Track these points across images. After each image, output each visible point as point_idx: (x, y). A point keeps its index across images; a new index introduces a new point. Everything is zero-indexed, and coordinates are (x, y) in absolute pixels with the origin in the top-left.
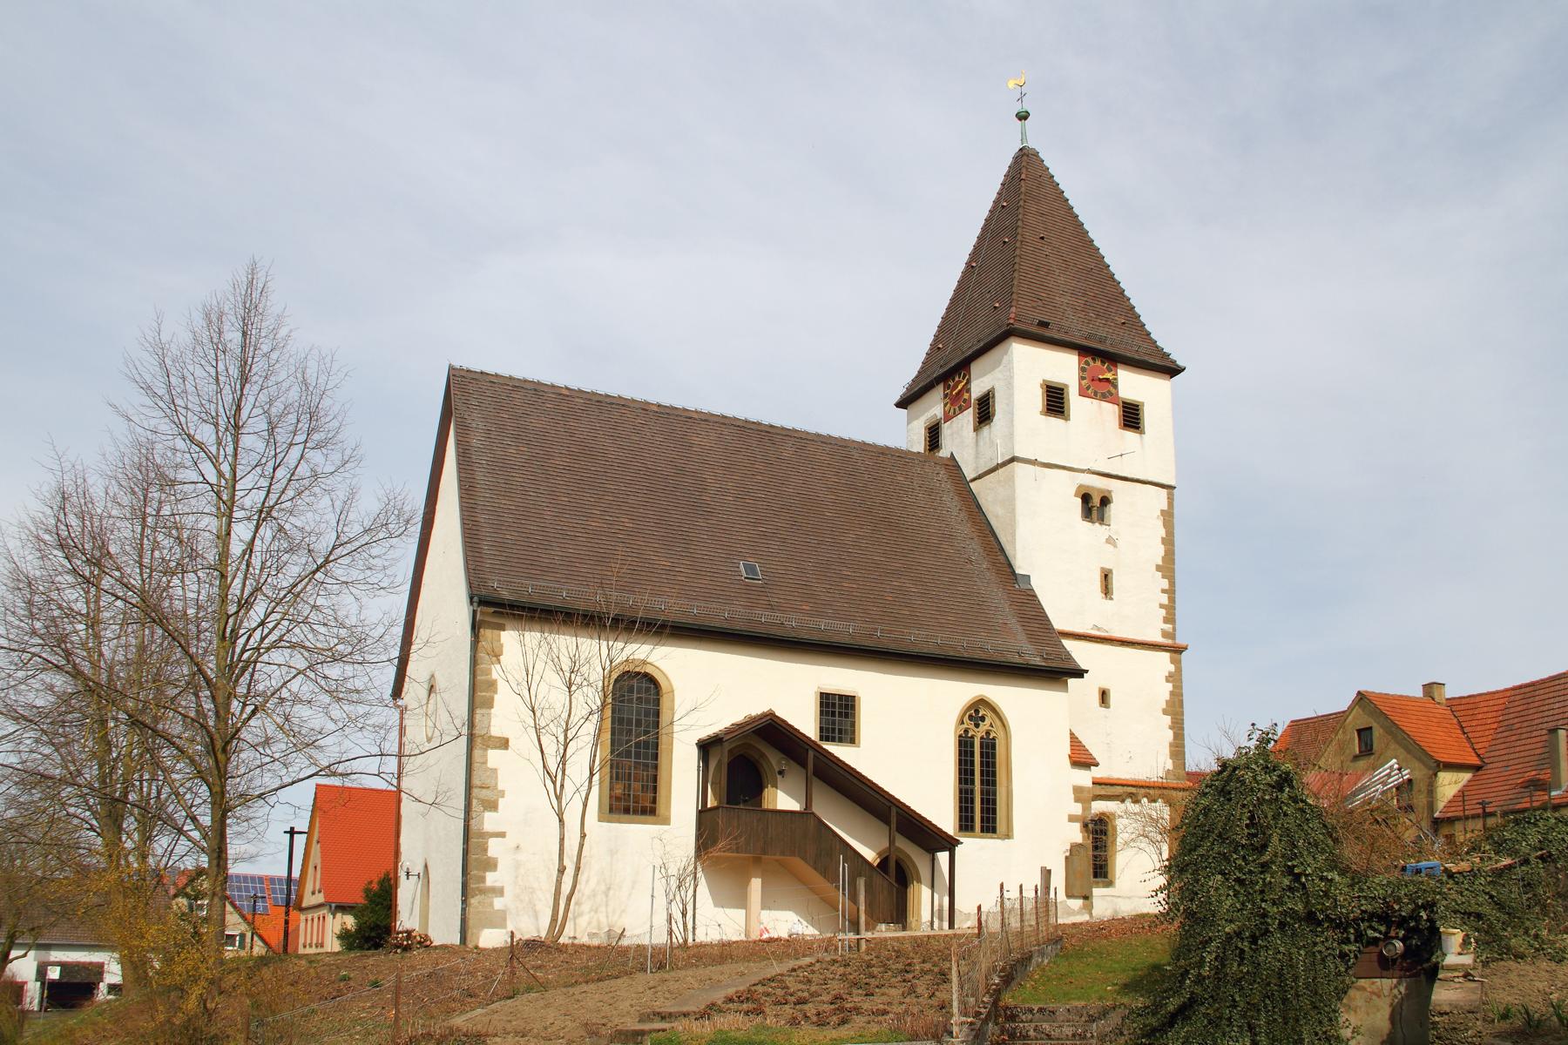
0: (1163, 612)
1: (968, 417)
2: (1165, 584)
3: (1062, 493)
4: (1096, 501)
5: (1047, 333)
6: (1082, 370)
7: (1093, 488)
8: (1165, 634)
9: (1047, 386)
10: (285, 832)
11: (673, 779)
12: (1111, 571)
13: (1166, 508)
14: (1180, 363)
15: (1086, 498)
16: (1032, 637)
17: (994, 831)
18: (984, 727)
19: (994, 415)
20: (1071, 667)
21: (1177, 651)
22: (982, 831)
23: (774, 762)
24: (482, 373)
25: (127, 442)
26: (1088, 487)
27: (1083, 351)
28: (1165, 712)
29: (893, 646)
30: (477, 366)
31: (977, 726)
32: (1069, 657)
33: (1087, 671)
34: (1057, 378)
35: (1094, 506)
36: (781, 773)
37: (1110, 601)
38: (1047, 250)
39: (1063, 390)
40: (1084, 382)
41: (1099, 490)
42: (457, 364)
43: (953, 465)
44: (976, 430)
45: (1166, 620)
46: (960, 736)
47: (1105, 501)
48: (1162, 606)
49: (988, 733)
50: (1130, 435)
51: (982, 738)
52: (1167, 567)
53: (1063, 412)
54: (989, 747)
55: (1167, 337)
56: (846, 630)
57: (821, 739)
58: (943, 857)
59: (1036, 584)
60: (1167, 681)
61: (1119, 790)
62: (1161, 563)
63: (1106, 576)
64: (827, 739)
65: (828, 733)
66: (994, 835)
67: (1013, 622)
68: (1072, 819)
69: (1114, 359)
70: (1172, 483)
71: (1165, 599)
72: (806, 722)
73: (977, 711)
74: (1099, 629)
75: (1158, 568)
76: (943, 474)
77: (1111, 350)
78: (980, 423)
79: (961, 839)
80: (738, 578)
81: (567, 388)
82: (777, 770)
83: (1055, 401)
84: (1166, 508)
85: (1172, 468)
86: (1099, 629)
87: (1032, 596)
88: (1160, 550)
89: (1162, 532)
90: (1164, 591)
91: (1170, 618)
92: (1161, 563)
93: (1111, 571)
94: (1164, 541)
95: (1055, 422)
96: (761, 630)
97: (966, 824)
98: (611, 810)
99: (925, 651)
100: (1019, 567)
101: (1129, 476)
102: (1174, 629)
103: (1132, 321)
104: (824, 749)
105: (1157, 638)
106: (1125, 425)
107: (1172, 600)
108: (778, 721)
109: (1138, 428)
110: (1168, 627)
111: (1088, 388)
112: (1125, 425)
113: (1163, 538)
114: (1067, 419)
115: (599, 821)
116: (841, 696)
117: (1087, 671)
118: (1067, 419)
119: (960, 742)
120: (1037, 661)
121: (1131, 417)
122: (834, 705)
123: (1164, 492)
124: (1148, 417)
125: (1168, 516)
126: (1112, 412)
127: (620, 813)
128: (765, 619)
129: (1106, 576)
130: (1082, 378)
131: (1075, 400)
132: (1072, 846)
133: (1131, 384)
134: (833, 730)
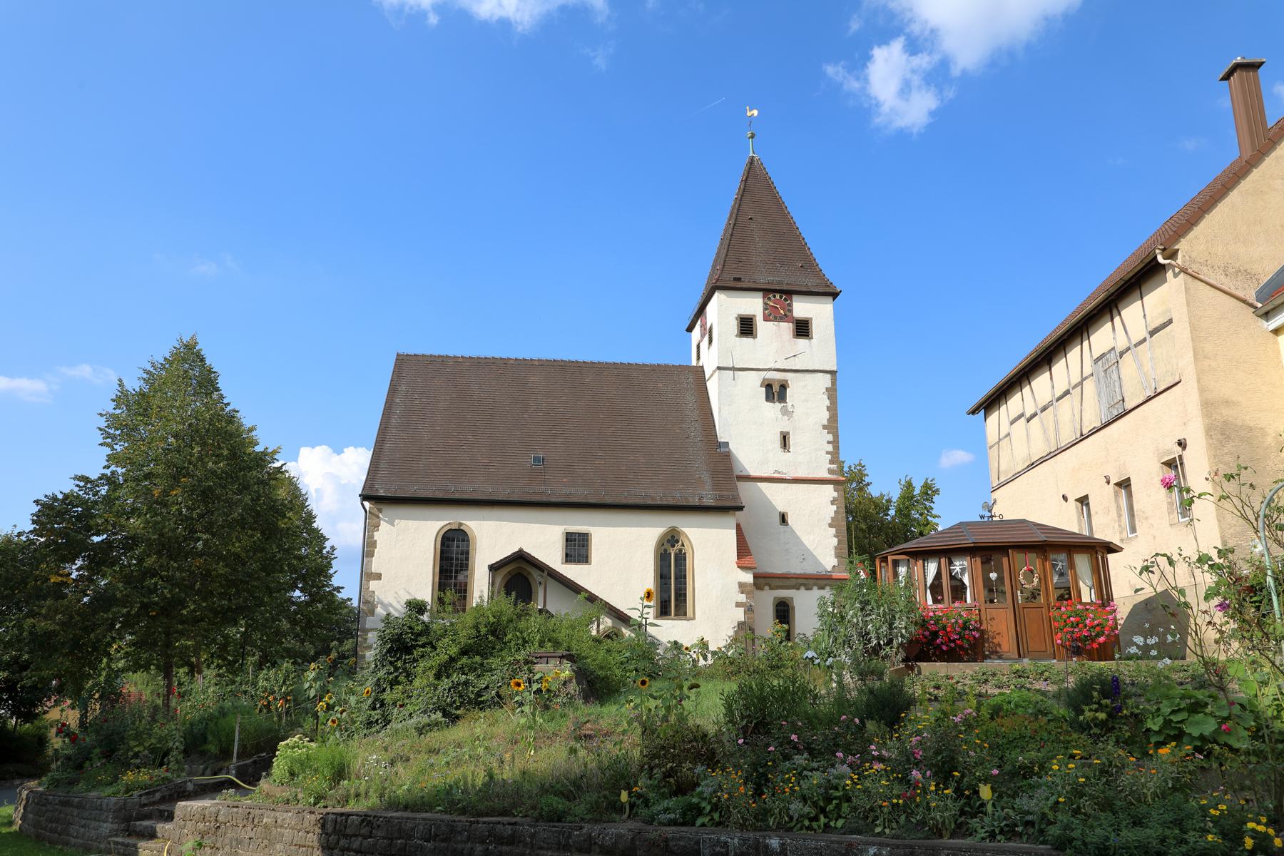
2: (830, 437)
3: (752, 384)
4: (776, 388)
5: (739, 285)
6: (765, 304)
8: (830, 471)
12: (788, 433)
13: (830, 386)
15: (768, 386)
18: (678, 546)
22: (676, 615)
27: (766, 292)
28: (831, 526)
31: (673, 546)
34: (746, 311)
35: (776, 392)
37: (788, 454)
41: (779, 381)
45: (831, 462)
47: (784, 387)
48: (828, 453)
49: (681, 550)
50: (802, 342)
52: (832, 426)
54: (681, 558)
55: (833, 274)
56: (580, 495)
60: (832, 504)
61: (793, 582)
63: (785, 437)
67: (706, 477)
68: (738, 605)
69: (789, 293)
71: (830, 448)
73: (672, 538)
74: (779, 473)
75: (824, 427)
81: (462, 357)
83: (747, 327)
84: (830, 386)
86: (779, 473)
88: (826, 415)
89: (827, 403)
90: (829, 442)
93: (788, 433)
94: (828, 408)
95: (747, 341)
100: (721, 438)
101: (810, 368)
105: (826, 475)
106: (797, 335)
107: (836, 448)
109: (808, 336)
111: (770, 315)
112: (797, 335)
113: (828, 407)
114: (755, 337)
118: (755, 337)
121: (803, 329)
123: (829, 376)
124: (815, 328)
125: (832, 392)
126: (787, 328)
129: (785, 439)
130: (765, 309)
131: (761, 326)
132: (739, 625)
133: (801, 308)
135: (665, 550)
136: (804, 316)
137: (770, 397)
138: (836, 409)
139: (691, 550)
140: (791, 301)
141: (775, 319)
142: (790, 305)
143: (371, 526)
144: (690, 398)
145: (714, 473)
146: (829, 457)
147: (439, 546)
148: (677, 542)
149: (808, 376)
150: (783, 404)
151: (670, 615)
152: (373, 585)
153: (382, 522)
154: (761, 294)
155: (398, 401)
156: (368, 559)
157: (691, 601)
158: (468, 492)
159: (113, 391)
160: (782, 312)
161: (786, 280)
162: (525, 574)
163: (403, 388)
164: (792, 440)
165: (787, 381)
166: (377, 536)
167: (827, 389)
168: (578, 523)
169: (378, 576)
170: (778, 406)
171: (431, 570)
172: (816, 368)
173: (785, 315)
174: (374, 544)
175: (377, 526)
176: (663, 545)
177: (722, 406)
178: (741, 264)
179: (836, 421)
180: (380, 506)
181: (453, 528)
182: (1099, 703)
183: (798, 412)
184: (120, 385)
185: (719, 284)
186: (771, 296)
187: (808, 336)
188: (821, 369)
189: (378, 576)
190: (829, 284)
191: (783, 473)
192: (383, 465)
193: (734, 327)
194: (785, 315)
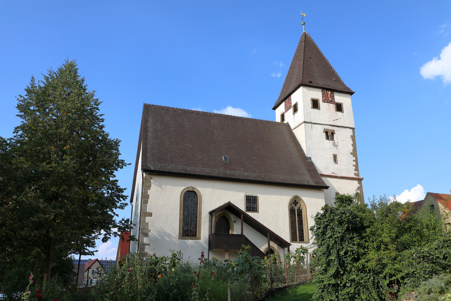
0: (354, 167)
1: (291, 110)
2: (354, 158)
3: (320, 130)
5: (312, 85)
6: (323, 94)
7: (329, 130)
9: (313, 100)
10: (102, 259)
11: (257, 246)
12: (336, 155)
13: (352, 135)
14: (353, 91)
15: (327, 133)
16: (312, 177)
17: (303, 240)
18: (298, 205)
19: (298, 109)
20: (324, 185)
21: (360, 180)
23: (232, 218)
24: (153, 105)
25: (98, 114)
26: (327, 129)
27: (324, 89)
29: (268, 180)
30: (151, 103)
31: (296, 205)
32: (323, 182)
33: (329, 187)
35: (329, 135)
36: (235, 222)
38: (311, 61)
39: (317, 101)
40: (324, 98)
41: (331, 130)
42: (146, 103)
43: (288, 125)
44: (294, 114)
45: (355, 170)
46: (291, 209)
47: (333, 133)
48: (354, 166)
49: (299, 208)
50: (339, 113)
51: (297, 209)
52: (354, 153)
53: (318, 107)
55: (349, 84)
56: (179, 168)
57: (247, 211)
58: (286, 249)
59: (313, 160)
62: (352, 152)
63: (335, 157)
64: (247, 211)
65: (249, 209)
66: (303, 242)
67: (306, 172)
69: (333, 91)
70: (354, 127)
71: (354, 163)
72: (241, 205)
73: (295, 202)
74: (334, 173)
75: (351, 154)
76: (285, 128)
77: (332, 88)
78: (294, 112)
79: (291, 243)
80: (222, 161)
81: (176, 108)
82: (233, 221)
83: (315, 104)
84: (352, 135)
85: (353, 122)
86: (334, 173)
87: (312, 164)
88: (351, 148)
89: (352, 142)
90: (354, 161)
91: (357, 169)
92: (352, 152)
93: (336, 155)
95: (316, 110)
96: (228, 176)
97: (294, 239)
98: (183, 236)
99: (277, 182)
100: (307, 155)
101: (344, 126)
102: (358, 173)
103: (338, 80)
104: (246, 214)
107: (357, 163)
108: (231, 205)
110: (356, 172)
111: (325, 100)
112: (337, 110)
113: (352, 144)
115: (179, 239)
116: (253, 197)
117: (329, 187)
119: (291, 211)
120: (313, 184)
121: (339, 108)
122: (250, 199)
124: (345, 107)
125: (353, 137)
126: (333, 106)
127: (186, 236)
128: (228, 173)
129: (335, 157)
130: (323, 97)
131: (322, 105)
133: (338, 98)
134: (251, 207)
135: (292, 207)
136: (340, 102)
137: (327, 138)
138: (355, 146)
139: (305, 207)
140: (334, 94)
141: (327, 102)
142: (333, 96)
143: (146, 186)
144: (288, 137)
145: (309, 171)
146: (354, 167)
147: (182, 200)
148: (297, 203)
149: (343, 129)
150: (333, 141)
151: (297, 241)
152: (148, 219)
153: (152, 185)
154: (320, 90)
155: (149, 125)
156: (145, 205)
157: (307, 234)
158: (197, 170)
159: (27, 84)
160: (330, 99)
161: (331, 86)
162: (227, 216)
163: (150, 120)
164: (338, 158)
165: (334, 131)
166: (149, 192)
167: (351, 136)
168: (252, 190)
169: (150, 215)
170: (331, 142)
171: (179, 212)
172: (346, 126)
173: (331, 100)
174: (148, 197)
175: (149, 187)
176: (291, 204)
177: (307, 140)
178: (310, 76)
179: (356, 151)
180: (151, 176)
181: (190, 190)
182: (376, 291)
183: (340, 145)
184: (32, 81)
185: (303, 83)
186: (325, 91)
187: (342, 111)
188: (348, 126)
189: (150, 215)
190: (348, 89)
191: (336, 174)
192: (149, 155)
193: (310, 104)
194: (331, 100)
